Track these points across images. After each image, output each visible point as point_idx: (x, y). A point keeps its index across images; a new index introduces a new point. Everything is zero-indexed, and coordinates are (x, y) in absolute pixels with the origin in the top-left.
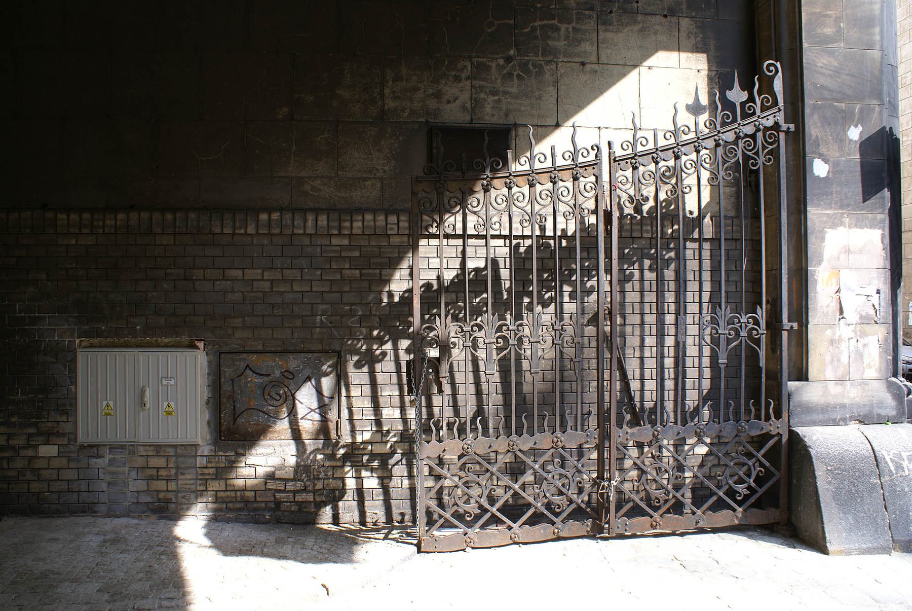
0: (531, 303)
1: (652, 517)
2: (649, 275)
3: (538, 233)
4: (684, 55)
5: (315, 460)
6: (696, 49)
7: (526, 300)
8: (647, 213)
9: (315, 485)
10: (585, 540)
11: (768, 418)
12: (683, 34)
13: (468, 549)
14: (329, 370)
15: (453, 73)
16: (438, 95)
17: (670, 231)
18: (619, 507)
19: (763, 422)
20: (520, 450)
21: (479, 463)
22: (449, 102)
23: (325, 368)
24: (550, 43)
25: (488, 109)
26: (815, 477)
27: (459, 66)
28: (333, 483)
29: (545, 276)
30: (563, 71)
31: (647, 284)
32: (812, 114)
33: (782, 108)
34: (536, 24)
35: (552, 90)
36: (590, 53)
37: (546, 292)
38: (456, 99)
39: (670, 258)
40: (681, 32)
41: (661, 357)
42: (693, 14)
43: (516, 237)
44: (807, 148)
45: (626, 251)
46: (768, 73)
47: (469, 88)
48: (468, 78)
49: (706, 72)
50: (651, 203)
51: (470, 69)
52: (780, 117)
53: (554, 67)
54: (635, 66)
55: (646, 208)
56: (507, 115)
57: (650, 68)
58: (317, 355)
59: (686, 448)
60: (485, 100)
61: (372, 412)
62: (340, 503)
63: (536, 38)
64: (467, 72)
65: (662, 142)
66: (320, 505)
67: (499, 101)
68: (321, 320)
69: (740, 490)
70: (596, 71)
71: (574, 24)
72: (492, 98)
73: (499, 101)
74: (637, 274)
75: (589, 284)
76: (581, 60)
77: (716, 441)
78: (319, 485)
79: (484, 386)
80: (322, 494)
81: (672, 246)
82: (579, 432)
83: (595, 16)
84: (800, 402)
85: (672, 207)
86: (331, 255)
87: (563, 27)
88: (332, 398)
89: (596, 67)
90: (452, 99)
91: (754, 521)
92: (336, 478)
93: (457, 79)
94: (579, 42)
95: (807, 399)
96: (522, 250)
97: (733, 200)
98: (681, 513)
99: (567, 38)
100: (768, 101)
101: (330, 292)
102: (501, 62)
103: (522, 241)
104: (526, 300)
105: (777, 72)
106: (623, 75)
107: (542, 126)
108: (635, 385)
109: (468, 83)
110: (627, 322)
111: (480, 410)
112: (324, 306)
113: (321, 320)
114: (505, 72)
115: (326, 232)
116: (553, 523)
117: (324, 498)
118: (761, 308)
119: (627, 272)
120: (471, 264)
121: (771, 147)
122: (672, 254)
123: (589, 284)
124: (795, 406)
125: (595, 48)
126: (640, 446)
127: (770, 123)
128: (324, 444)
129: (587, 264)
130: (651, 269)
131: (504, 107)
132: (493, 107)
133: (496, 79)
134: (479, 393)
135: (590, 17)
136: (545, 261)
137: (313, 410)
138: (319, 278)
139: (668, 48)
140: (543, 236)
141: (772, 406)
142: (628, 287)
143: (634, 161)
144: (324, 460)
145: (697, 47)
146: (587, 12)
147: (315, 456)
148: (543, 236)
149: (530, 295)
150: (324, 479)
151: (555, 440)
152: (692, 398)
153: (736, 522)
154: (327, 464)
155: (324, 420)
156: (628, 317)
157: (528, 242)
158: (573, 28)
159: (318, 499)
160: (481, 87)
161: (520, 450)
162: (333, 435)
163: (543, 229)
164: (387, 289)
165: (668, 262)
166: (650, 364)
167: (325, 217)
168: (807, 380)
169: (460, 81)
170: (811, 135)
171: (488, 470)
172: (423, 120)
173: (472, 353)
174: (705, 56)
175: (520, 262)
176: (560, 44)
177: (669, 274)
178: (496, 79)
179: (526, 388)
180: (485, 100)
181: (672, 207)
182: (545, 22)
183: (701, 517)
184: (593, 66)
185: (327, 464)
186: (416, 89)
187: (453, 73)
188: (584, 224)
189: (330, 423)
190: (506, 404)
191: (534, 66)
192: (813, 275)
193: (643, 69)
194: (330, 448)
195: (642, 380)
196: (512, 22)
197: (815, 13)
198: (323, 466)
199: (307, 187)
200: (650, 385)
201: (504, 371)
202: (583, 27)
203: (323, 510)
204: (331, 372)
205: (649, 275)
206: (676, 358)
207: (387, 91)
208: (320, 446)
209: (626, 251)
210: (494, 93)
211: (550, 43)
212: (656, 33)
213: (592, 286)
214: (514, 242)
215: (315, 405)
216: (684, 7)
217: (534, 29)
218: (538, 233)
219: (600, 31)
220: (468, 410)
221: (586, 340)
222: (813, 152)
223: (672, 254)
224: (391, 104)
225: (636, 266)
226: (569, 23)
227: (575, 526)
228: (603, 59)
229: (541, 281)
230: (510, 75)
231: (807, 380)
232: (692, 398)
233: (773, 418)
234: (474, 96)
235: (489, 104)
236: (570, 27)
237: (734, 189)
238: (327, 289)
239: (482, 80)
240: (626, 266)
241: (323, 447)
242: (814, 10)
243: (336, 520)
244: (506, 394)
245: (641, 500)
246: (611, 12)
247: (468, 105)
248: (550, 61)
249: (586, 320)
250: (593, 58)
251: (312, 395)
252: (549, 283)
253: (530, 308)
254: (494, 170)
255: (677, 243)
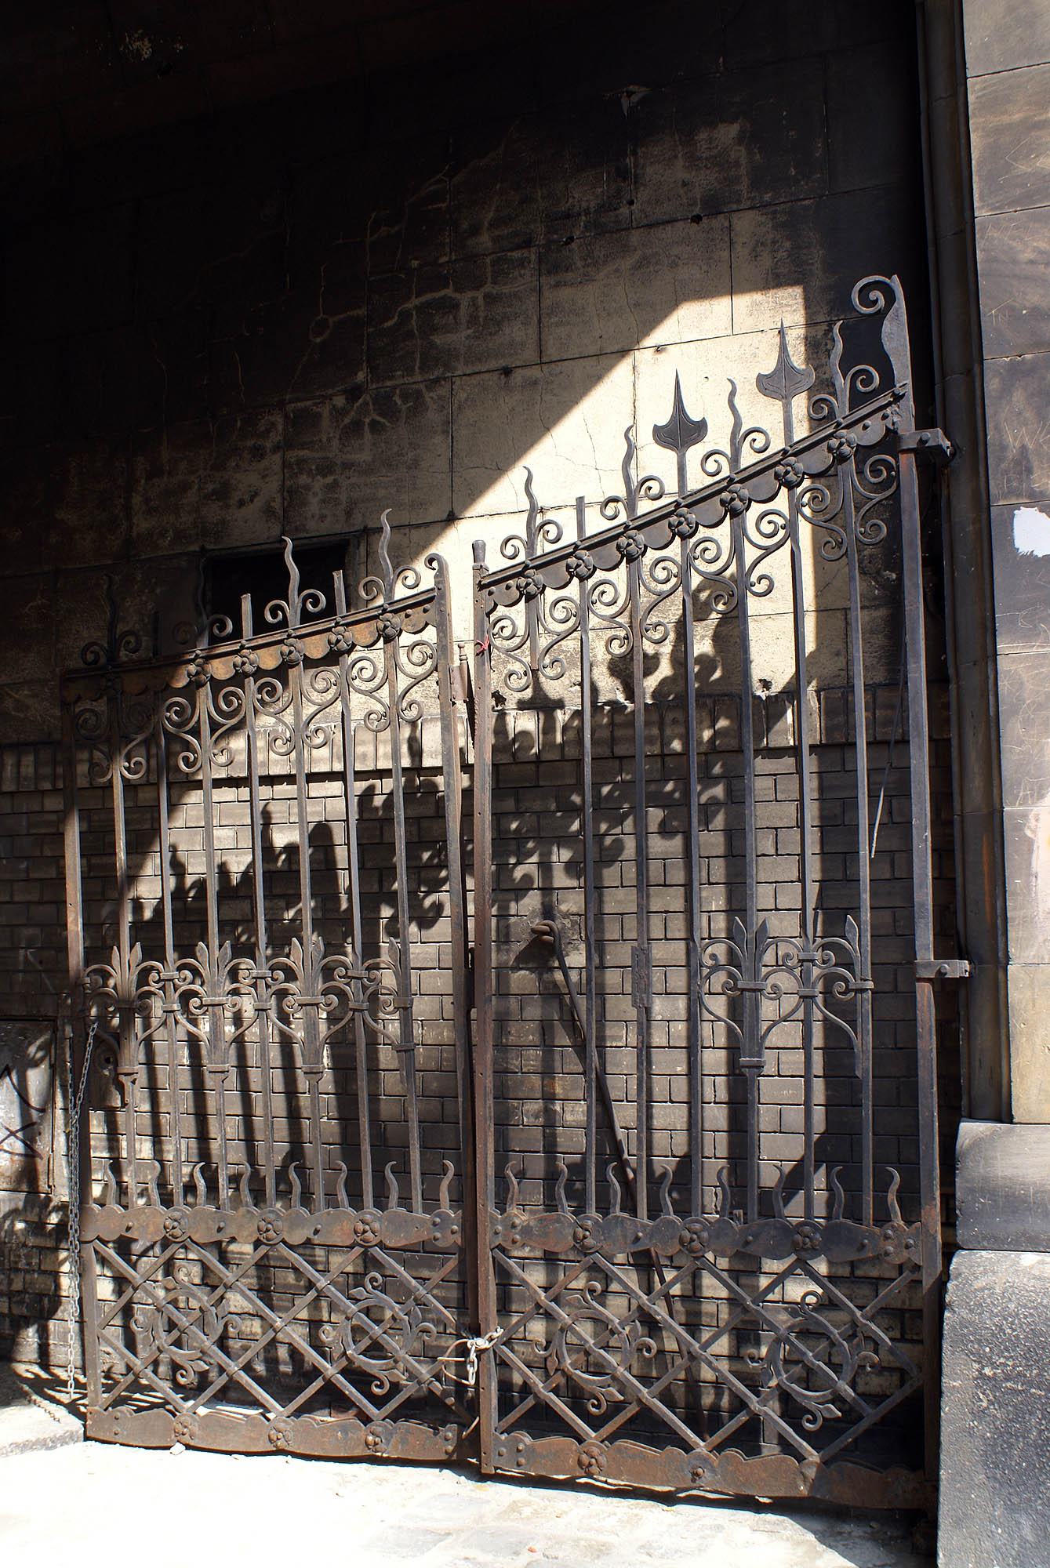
0: (394, 919)
1: (580, 1440)
2: (657, 845)
3: (406, 762)
4: (743, 301)
5: (11, 1231)
6: (774, 280)
7: (386, 912)
8: (654, 695)
9: (10, 1283)
10: (364, 1465)
11: (882, 1218)
12: (742, 252)
13: (178, 1448)
14: (40, 1054)
15: (250, 443)
16: (222, 494)
17: (707, 734)
18: (505, 1406)
19: (868, 1226)
20: (381, 1245)
21: (296, 1269)
22: (241, 503)
23: (32, 1050)
24: (438, 340)
25: (314, 505)
26: (940, 1394)
27: (262, 427)
28: (40, 1282)
29: (426, 856)
30: (463, 396)
31: (655, 868)
32: (1006, 391)
33: (909, 391)
34: (408, 305)
35: (440, 442)
36: (523, 344)
37: (428, 894)
38: (256, 494)
39: (714, 802)
40: (738, 247)
41: (693, 1047)
42: (767, 197)
43: (360, 775)
44: (992, 483)
45: (605, 790)
46: (865, 310)
47: (277, 468)
48: (276, 448)
49: (802, 332)
50: (665, 670)
51: (280, 428)
52: (903, 417)
53: (443, 390)
54: (624, 353)
55: (651, 683)
56: (349, 513)
57: (659, 349)
58: (19, 1025)
59: (764, 1282)
60: (308, 488)
61: (105, 1144)
62: (51, 1324)
63: (410, 335)
64: (275, 437)
65: (596, 524)
66: (19, 1323)
67: (335, 485)
68: (26, 956)
69: (812, 1405)
70: (535, 383)
71: (488, 288)
72: (320, 482)
73: (335, 485)
74: (630, 845)
75: (518, 873)
76: (502, 363)
77: (845, 1271)
78: (18, 1285)
79: (304, 1100)
80: (22, 1302)
81: (717, 770)
82: (419, 1214)
83: (533, 257)
84: (986, 1179)
85: (717, 674)
86: (43, 831)
87: (465, 299)
88: (42, 1110)
89: (535, 373)
90: (247, 497)
91: (845, 1495)
92: (45, 1272)
93: (258, 453)
94: (499, 324)
95: (1008, 1172)
96: (378, 801)
97: (879, 640)
98: (753, 1450)
99: (473, 320)
100: (869, 380)
101: (40, 903)
102: (340, 401)
103: (377, 782)
104: (386, 912)
105: (890, 298)
106: (596, 378)
107: (418, 526)
108: (625, 1115)
109: (277, 458)
110: (609, 959)
111: (296, 1152)
112: (31, 931)
113: (26, 956)
114: (347, 421)
115: (32, 788)
116: (366, 1419)
117: (24, 1311)
118: (857, 919)
119: (608, 840)
120: (280, 839)
121: (878, 497)
122: (718, 791)
123: (518, 873)
124: (972, 1190)
125: (532, 331)
126: (645, 1263)
127: (874, 431)
128: (26, 1201)
129: (514, 826)
130: (665, 831)
131: (343, 498)
132: (323, 501)
133: (329, 440)
134: (294, 1115)
135: (522, 263)
136: (425, 824)
137: (13, 1134)
138: (23, 876)
139: (704, 292)
140: (417, 769)
141: (894, 1187)
142: (610, 875)
143: (522, 581)
144: (25, 1231)
145: (777, 276)
146: (516, 254)
147: (12, 1224)
148: (417, 769)
149: (392, 899)
150: (27, 1271)
151: (361, 1227)
152: (778, 1150)
153: (803, 1489)
154: (32, 1241)
155: (30, 1154)
156: (610, 948)
157: (387, 785)
158: (487, 296)
159: (16, 1311)
160: (301, 462)
161: (381, 1245)
162: (43, 1186)
163: (416, 751)
164: (131, 895)
165: (707, 812)
166: (670, 1064)
167: (31, 758)
168: (1010, 1120)
169: (262, 456)
170: (1003, 448)
171: (311, 1285)
172: (195, 548)
173: (740, 1023)
174: (797, 292)
175: (373, 824)
176: (458, 338)
177: (711, 840)
178: (329, 440)
179: (387, 1109)
180: (308, 488)
181: (717, 674)
182: (428, 297)
183: (705, 1460)
184: (528, 372)
185: (32, 1241)
186: (185, 487)
187: (250, 443)
188: (505, 732)
189: (38, 1160)
190: (349, 1145)
191: (405, 397)
192: (1019, 828)
193: (643, 356)
194: (37, 1210)
195: (647, 1102)
196: (361, 312)
197: (1010, 126)
198: (25, 1245)
199: (9, 704)
200: (670, 1117)
201: (344, 1068)
202: (506, 290)
203: (23, 1333)
204: (42, 1060)
205: (657, 845)
206: (733, 1050)
207: (137, 500)
208: (21, 1205)
209: (605, 790)
210: (326, 469)
211: (438, 340)
212: (674, 265)
213: (527, 877)
214: (360, 786)
215: (16, 1125)
216: (744, 186)
217: (406, 316)
218: (406, 762)
219: (545, 288)
220: (274, 1151)
221: (513, 1003)
222: (1012, 492)
223: (718, 791)
224: (143, 524)
225: (629, 825)
226: (477, 288)
227: (416, 1434)
228: (552, 352)
229: (415, 869)
230: (356, 427)
231: (1010, 1120)
232: (778, 1150)
233: (899, 1221)
234: (288, 483)
235: (315, 494)
236: (479, 295)
237: (882, 612)
238: (35, 897)
239: (303, 447)
240: (603, 827)
241: (25, 1206)
242: (1006, 119)
243: (44, 1358)
244: (347, 1116)
245: (556, 1391)
246: (571, 239)
247: (277, 505)
248: (437, 381)
249: (513, 957)
250: (530, 354)
251: (12, 1103)
252: (431, 874)
253: (393, 930)
254: (214, 641)
255: (731, 760)
